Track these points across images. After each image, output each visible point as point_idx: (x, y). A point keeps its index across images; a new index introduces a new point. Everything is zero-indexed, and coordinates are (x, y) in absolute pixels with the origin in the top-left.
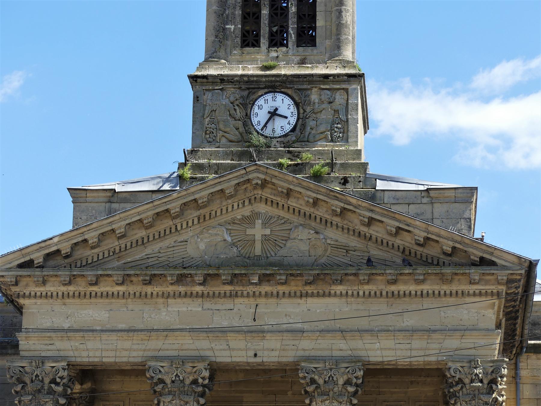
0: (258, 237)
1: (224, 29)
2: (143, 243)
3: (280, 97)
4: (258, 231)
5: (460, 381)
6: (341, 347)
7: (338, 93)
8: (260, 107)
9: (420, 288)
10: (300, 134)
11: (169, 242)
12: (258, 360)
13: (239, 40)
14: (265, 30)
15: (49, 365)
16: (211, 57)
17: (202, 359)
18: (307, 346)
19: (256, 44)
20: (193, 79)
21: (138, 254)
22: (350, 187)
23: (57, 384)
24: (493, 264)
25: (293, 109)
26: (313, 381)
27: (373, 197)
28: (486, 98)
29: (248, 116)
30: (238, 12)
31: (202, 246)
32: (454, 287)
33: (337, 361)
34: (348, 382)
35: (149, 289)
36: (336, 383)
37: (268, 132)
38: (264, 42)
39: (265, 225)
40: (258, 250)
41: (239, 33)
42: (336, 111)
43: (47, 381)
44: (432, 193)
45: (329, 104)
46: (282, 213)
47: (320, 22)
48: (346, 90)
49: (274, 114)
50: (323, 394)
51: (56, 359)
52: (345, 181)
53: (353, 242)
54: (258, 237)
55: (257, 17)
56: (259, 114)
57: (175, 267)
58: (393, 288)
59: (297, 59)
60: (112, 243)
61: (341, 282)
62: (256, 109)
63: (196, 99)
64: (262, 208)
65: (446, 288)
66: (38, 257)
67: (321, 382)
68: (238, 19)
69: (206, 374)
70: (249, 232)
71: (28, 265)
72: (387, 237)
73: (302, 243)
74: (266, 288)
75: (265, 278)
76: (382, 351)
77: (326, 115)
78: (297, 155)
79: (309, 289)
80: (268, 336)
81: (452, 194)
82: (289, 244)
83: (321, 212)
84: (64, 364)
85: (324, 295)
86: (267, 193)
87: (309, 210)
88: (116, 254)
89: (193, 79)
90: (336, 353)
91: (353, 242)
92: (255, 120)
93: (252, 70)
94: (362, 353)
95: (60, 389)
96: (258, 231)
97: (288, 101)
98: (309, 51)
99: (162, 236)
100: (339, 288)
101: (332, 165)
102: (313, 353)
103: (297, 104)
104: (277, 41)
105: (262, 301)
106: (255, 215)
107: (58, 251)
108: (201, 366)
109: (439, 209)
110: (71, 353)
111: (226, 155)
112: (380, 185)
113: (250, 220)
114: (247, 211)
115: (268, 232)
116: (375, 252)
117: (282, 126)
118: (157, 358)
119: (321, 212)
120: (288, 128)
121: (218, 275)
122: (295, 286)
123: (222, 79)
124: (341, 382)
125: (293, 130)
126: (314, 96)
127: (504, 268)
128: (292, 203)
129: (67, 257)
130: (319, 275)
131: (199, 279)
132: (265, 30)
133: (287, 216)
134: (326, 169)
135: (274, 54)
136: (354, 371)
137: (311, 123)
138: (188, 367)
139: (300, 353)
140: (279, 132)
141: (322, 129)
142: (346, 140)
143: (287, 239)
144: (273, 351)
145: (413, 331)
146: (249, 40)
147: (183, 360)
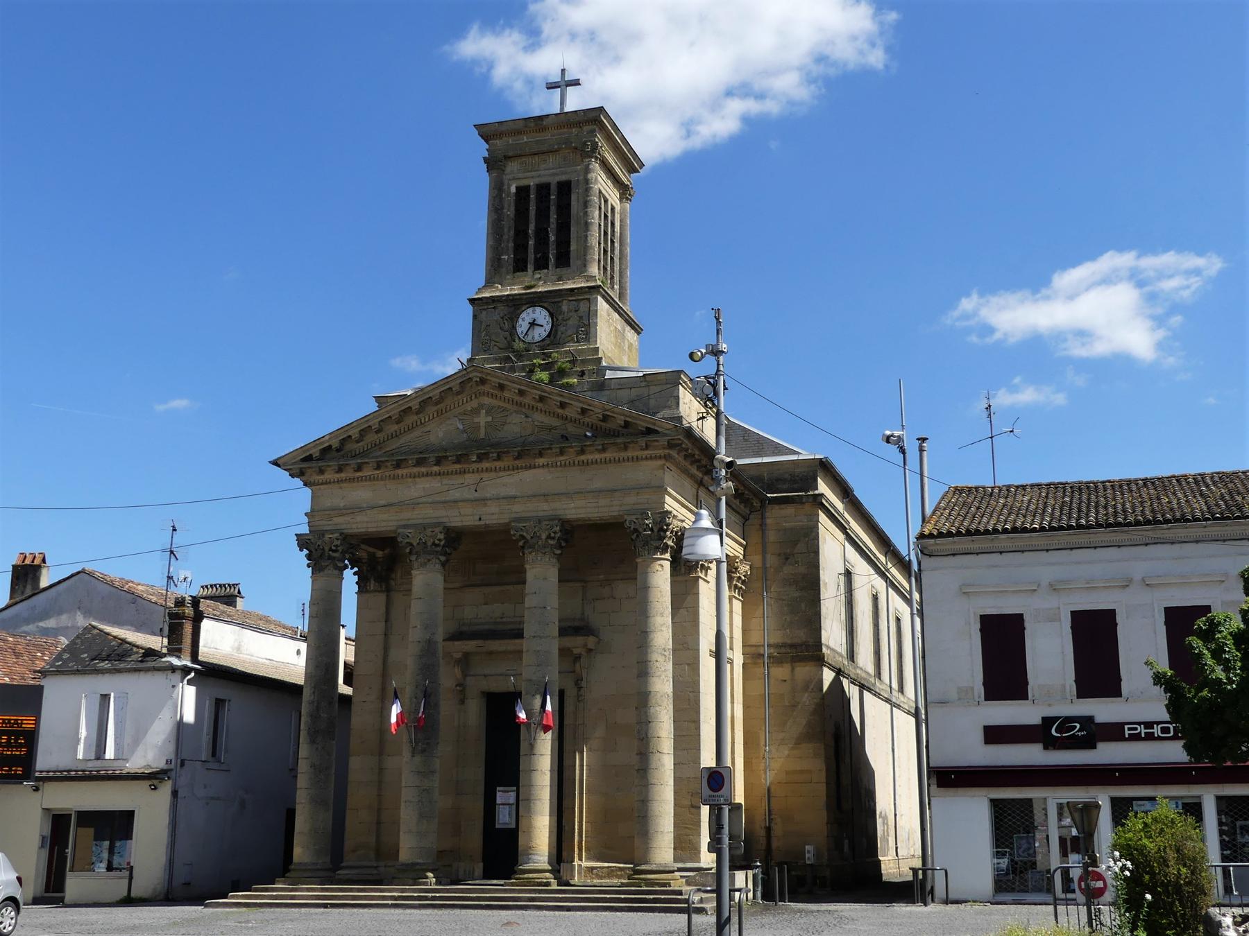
0: (483, 424)
1: (499, 259)
2: (396, 435)
3: (538, 309)
4: (482, 419)
5: (636, 530)
6: (544, 508)
7: (581, 304)
8: (523, 319)
9: (603, 456)
10: (553, 339)
11: (417, 433)
12: (482, 523)
13: (511, 268)
14: (531, 257)
15: (328, 536)
16: (489, 283)
17: (439, 524)
18: (519, 509)
19: (524, 269)
20: (472, 301)
21: (394, 445)
22: (586, 378)
23: (553, 538)
24: (657, 432)
25: (548, 319)
26: (523, 537)
27: (602, 386)
28: (1072, 297)
29: (514, 327)
30: (511, 245)
31: (441, 434)
32: (630, 454)
33: (540, 521)
34: (549, 537)
35: (400, 472)
36: (539, 538)
37: (529, 339)
38: (530, 267)
39: (488, 413)
40: (482, 434)
41: (511, 261)
42: (581, 318)
43: (327, 549)
44: (648, 378)
45: (572, 315)
46: (502, 404)
47: (573, 247)
48: (589, 300)
49: (533, 324)
50: (532, 547)
51: (332, 531)
52: (582, 374)
53: (555, 422)
54: (483, 424)
55: (526, 247)
56: (522, 326)
57: (414, 453)
58: (583, 457)
59: (554, 278)
60: (371, 438)
61: (541, 455)
62: (520, 321)
63: (475, 317)
64: (487, 401)
65: (624, 455)
66: (316, 454)
67: (528, 537)
68: (511, 251)
69: (441, 536)
70: (476, 420)
71: (308, 459)
72: (578, 417)
73: (515, 426)
74: (485, 465)
75: (481, 458)
76: (577, 509)
77: (573, 322)
78: (547, 356)
79: (519, 463)
80: (489, 502)
81: (663, 377)
82: (506, 428)
83: (527, 400)
84: (440, 529)
85: (530, 468)
86: (487, 388)
87: (517, 398)
88: (378, 445)
89: (472, 301)
90: (541, 514)
91: (555, 422)
92: (519, 330)
93: (517, 290)
94: (559, 513)
95: (439, 549)
96: (482, 419)
97: (545, 313)
98: (564, 271)
99: (410, 429)
100: (541, 461)
101: (573, 362)
102: (524, 515)
103: (551, 315)
104: (541, 265)
105: (485, 476)
106: (481, 406)
107: (330, 446)
108: (437, 530)
109: (654, 389)
110: (343, 527)
111: (495, 360)
112: (609, 374)
113: (476, 412)
114: (474, 404)
115: (490, 419)
116: (571, 429)
117: (539, 334)
118: (406, 526)
119: (527, 400)
120: (544, 334)
121: (446, 457)
122: (507, 462)
123: (493, 300)
124: (544, 537)
125: (549, 336)
126: (564, 307)
127: (665, 435)
128: (506, 394)
129: (338, 450)
130: (524, 452)
131: (432, 460)
132: (531, 257)
133: (505, 405)
134: (568, 365)
135: (538, 276)
136: (552, 527)
137: (562, 329)
138: (429, 531)
139: (513, 515)
140: (537, 338)
141: (569, 332)
142: (587, 340)
143: (505, 423)
144: (493, 515)
145: (598, 492)
146: (520, 266)
147: (424, 527)
